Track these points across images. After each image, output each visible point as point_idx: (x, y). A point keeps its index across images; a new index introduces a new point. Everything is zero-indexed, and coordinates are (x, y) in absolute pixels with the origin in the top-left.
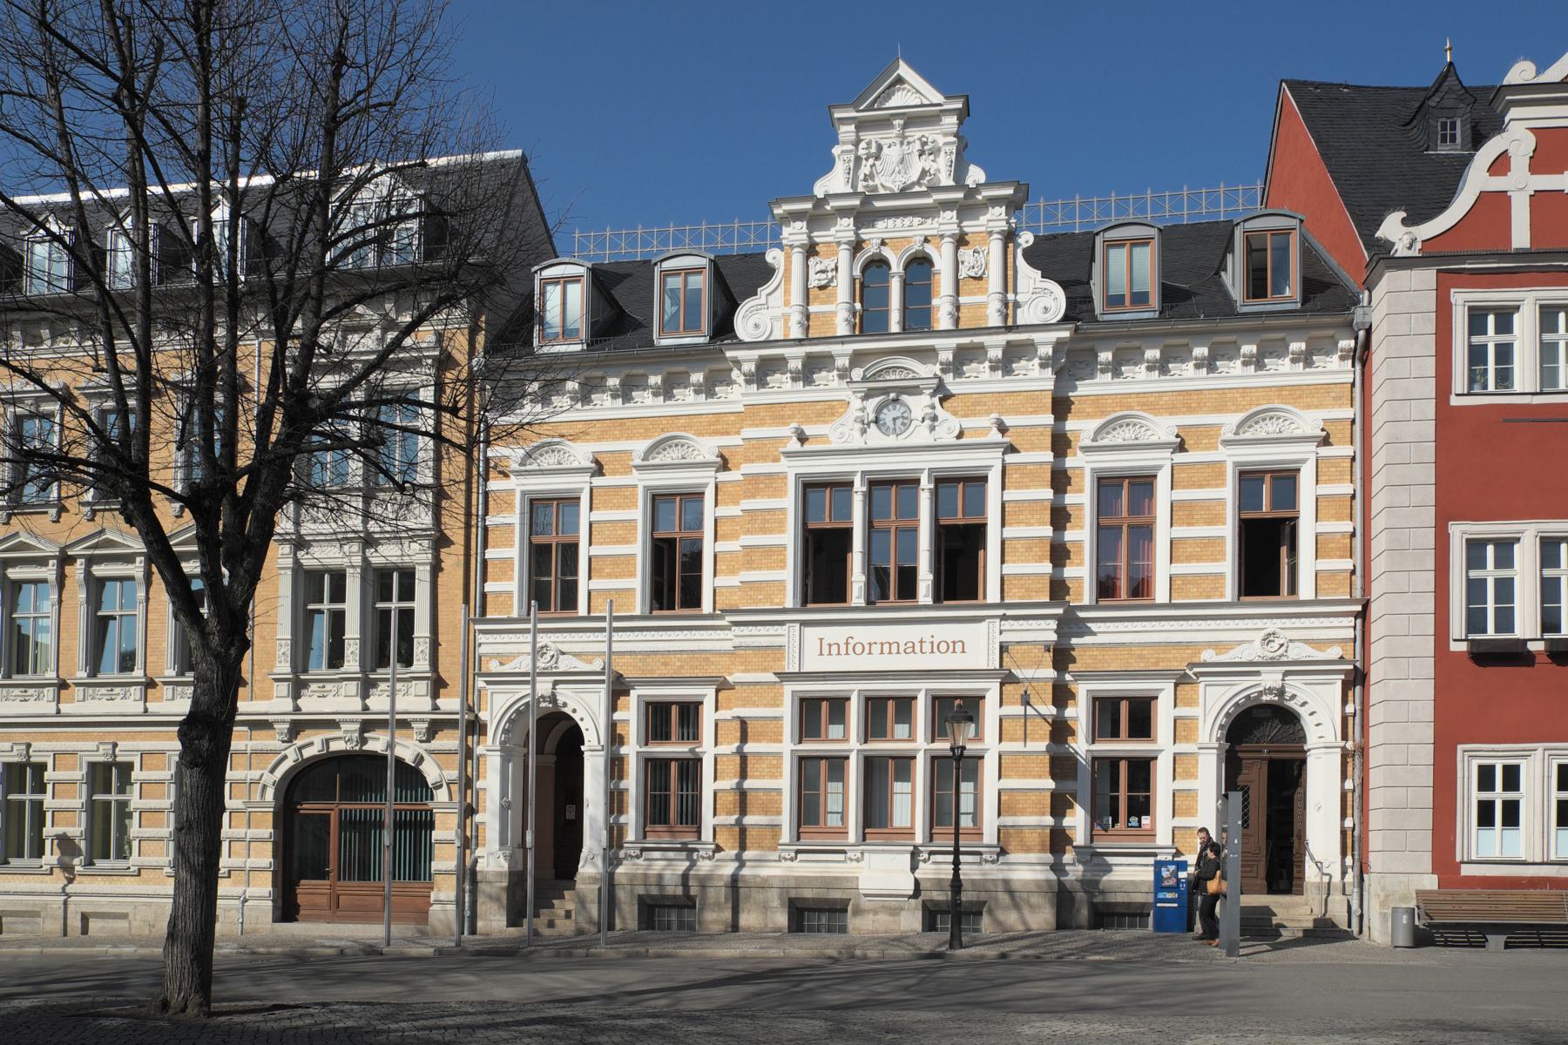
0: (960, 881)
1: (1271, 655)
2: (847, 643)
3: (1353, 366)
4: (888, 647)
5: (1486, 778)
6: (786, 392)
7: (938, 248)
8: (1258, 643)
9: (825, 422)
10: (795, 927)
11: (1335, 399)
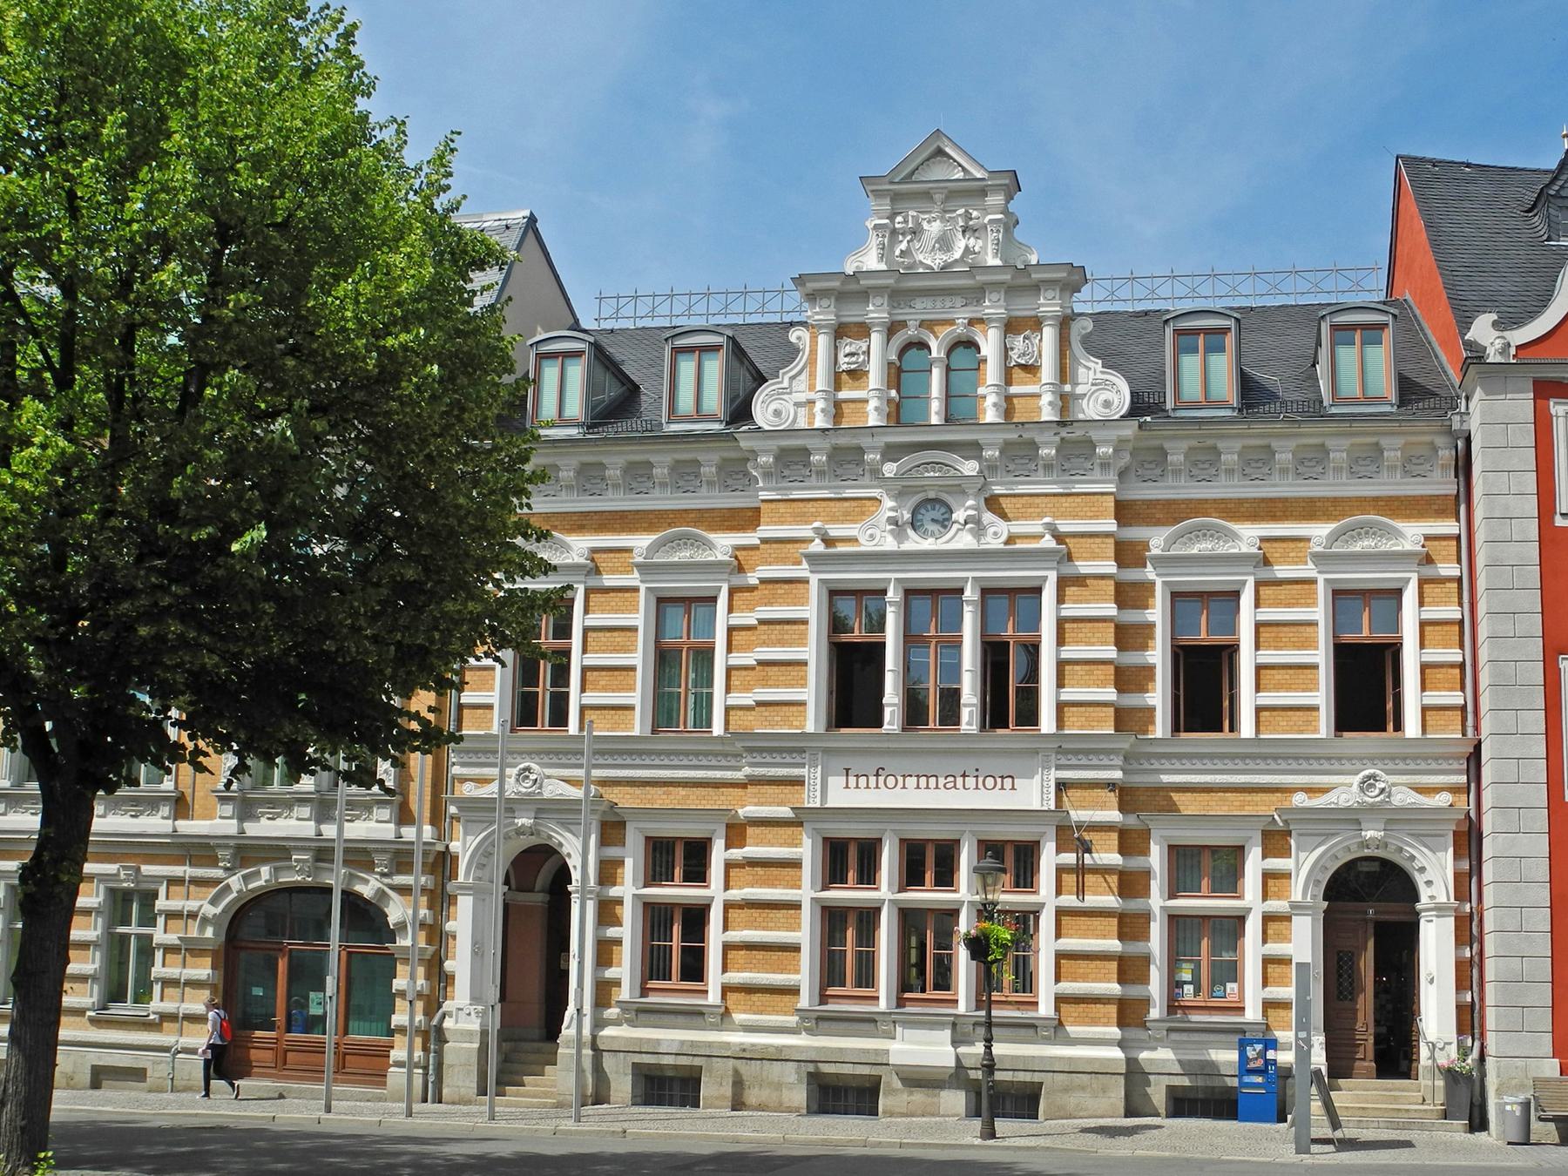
3: (1456, 476)
6: (562, 502)
7: (985, 333)
8: (1355, 788)
10: (815, 1107)
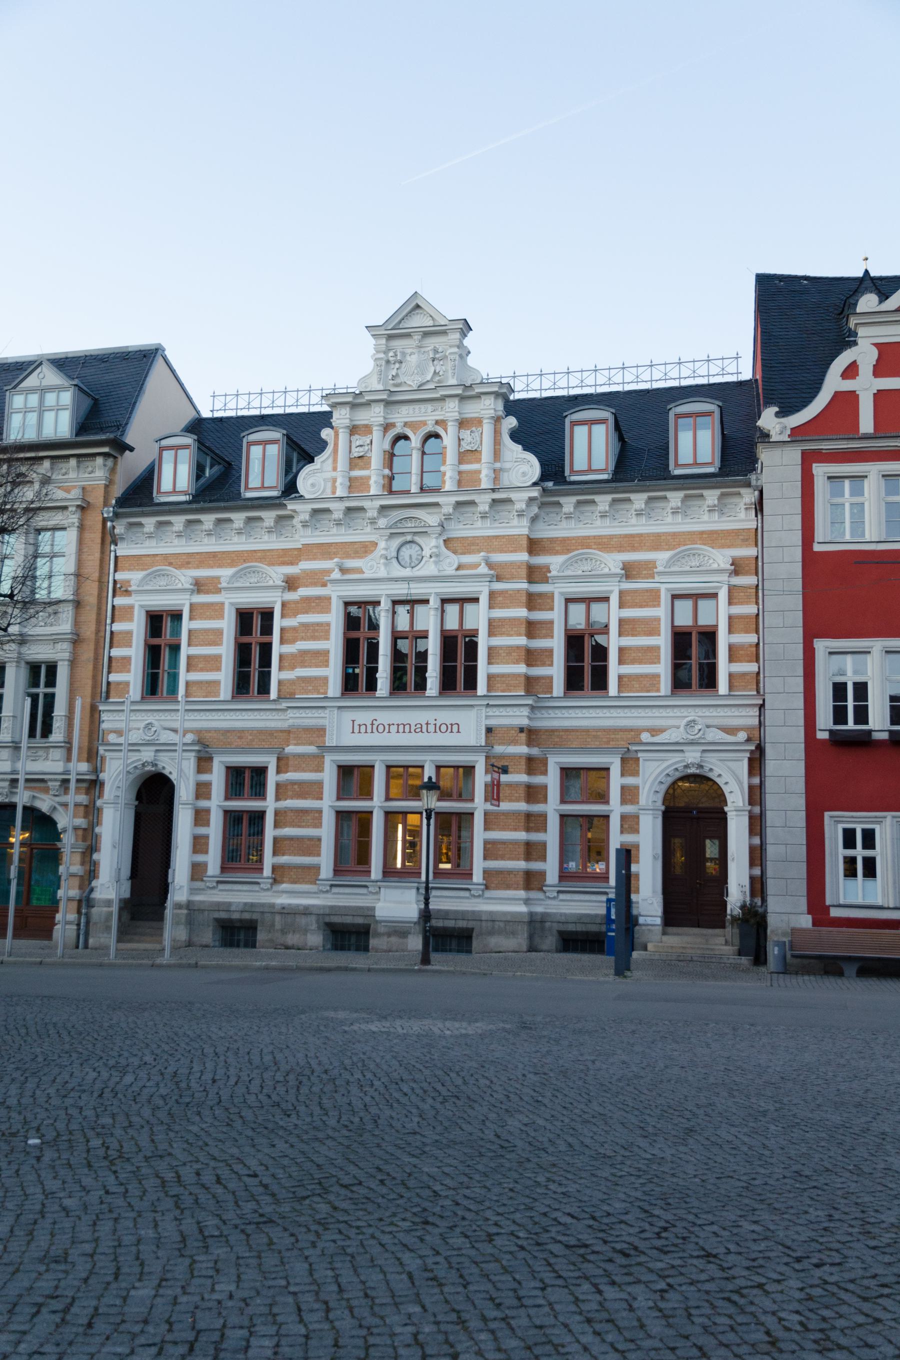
0: (429, 912)
1: (692, 737)
2: (372, 724)
3: (756, 516)
4: (403, 728)
5: (849, 839)
6: (333, 535)
8: (682, 728)
9: (361, 558)
11: (743, 540)
